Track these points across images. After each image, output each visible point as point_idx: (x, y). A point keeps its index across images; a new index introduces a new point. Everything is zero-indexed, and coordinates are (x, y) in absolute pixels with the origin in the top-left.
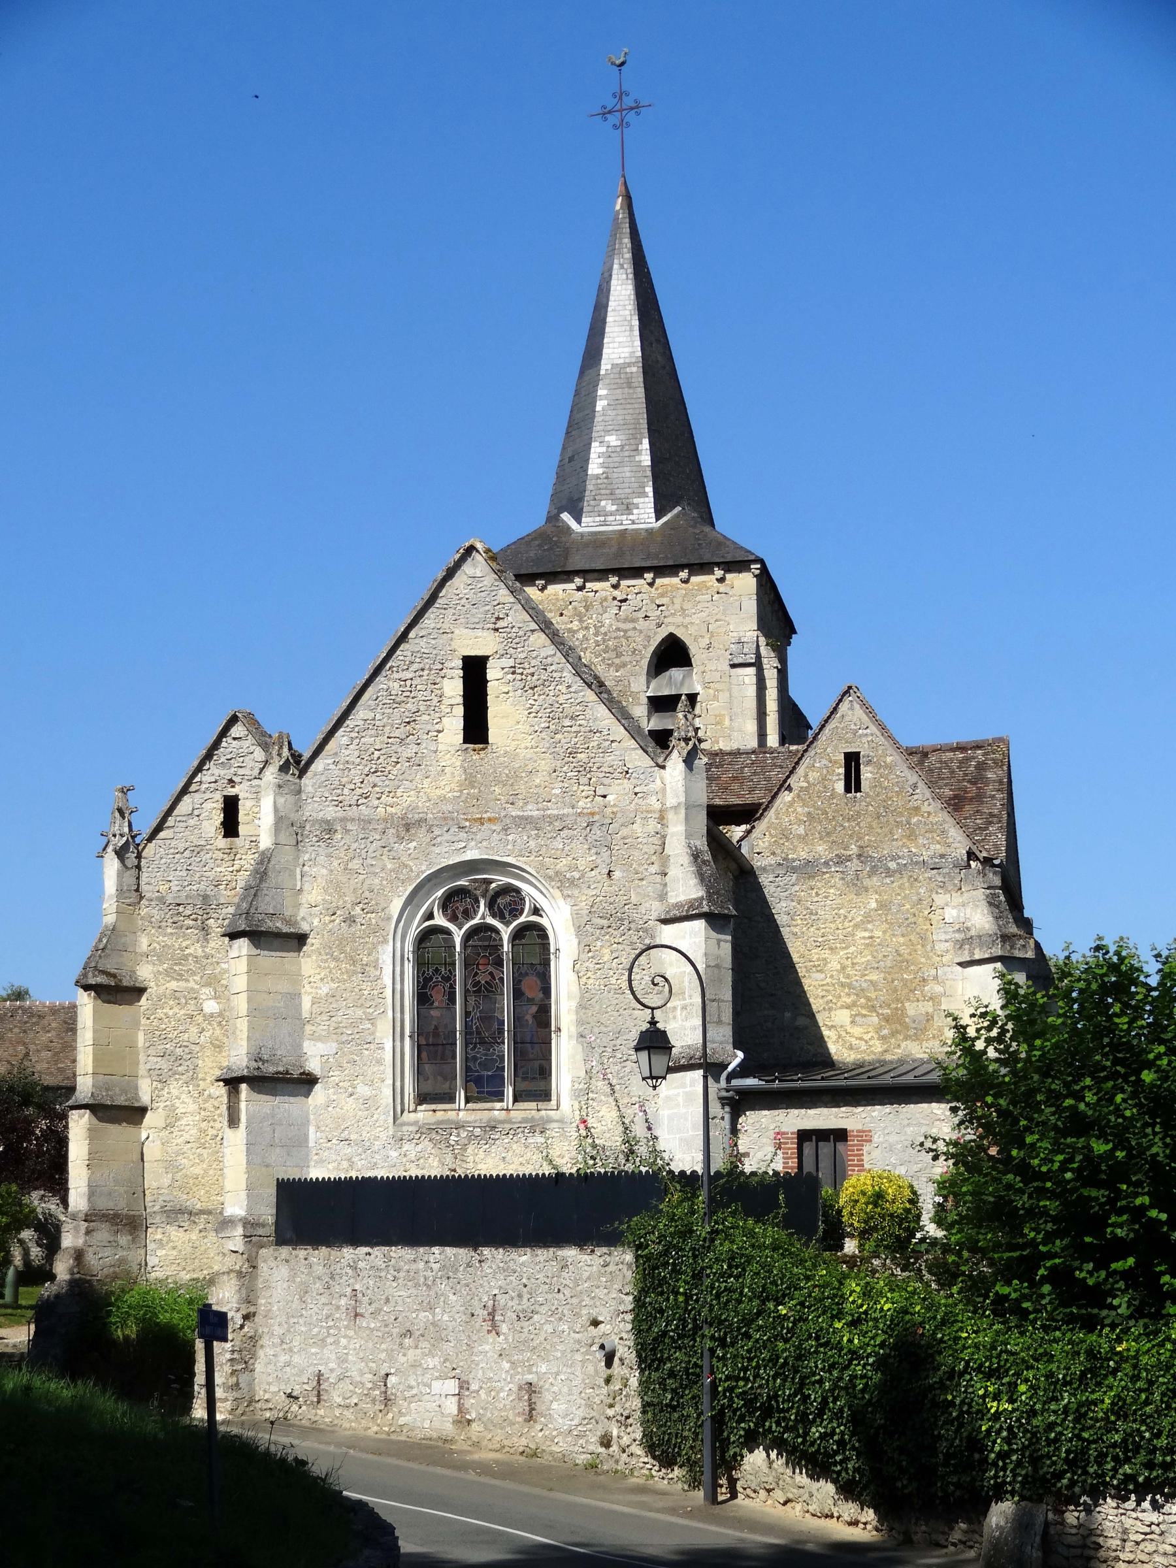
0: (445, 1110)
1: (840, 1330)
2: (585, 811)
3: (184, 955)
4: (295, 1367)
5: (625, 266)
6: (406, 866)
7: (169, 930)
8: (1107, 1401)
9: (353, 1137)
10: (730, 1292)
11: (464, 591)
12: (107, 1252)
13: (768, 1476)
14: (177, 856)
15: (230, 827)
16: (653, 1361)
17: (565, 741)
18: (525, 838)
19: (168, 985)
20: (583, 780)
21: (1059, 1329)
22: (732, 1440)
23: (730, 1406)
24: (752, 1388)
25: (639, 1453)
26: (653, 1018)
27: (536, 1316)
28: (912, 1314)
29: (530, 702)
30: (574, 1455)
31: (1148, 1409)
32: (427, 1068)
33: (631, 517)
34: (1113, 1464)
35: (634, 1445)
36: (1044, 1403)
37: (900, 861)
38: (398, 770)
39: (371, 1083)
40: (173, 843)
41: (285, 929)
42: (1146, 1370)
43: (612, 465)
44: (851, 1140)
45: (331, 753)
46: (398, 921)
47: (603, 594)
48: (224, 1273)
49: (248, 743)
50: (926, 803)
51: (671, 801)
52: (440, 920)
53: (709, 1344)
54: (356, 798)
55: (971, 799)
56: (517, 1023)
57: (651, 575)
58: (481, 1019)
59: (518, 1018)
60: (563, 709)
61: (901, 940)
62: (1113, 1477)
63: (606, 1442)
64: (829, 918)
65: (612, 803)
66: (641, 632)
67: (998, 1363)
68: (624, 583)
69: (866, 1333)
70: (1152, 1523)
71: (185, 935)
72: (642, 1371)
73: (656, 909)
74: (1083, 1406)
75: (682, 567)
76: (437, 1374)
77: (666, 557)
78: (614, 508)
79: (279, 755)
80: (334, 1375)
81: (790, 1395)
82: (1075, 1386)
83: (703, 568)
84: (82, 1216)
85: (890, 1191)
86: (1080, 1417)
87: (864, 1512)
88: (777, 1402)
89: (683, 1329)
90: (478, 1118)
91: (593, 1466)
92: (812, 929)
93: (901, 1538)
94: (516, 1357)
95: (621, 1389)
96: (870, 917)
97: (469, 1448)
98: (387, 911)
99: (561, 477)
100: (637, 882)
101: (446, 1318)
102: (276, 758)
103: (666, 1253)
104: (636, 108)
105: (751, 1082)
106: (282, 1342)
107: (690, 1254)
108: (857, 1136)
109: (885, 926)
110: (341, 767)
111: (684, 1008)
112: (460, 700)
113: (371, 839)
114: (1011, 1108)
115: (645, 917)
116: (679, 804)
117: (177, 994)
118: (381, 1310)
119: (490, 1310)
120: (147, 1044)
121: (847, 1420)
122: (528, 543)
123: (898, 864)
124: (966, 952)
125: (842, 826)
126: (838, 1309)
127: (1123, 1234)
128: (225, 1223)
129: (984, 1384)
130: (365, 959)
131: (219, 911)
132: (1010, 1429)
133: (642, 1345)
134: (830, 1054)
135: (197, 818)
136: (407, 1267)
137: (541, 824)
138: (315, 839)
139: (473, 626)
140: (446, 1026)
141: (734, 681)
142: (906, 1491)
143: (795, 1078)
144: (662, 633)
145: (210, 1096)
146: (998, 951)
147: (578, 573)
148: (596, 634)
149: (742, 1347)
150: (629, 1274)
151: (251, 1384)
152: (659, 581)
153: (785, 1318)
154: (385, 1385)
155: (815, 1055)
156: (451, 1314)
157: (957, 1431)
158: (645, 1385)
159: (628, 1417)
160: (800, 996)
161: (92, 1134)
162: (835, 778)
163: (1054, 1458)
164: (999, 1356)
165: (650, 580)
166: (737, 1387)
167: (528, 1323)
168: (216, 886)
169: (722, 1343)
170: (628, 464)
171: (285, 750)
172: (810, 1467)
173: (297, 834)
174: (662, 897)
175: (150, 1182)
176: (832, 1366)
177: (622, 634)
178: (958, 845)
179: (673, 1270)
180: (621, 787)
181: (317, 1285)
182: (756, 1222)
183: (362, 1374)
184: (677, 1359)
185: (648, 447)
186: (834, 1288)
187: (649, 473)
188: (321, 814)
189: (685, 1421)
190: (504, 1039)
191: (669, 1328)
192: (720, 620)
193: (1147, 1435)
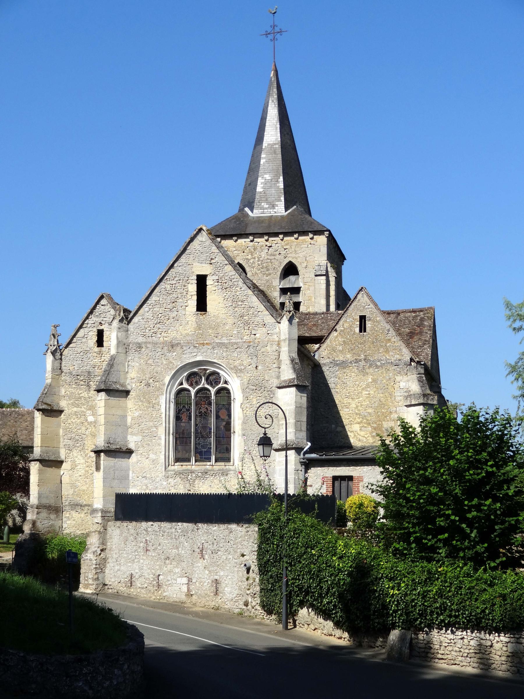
1: (335, 561)
2: (247, 341)
5: (274, 101)
6: (172, 363)
7: (74, 386)
8: (434, 591)
9: (148, 476)
10: (294, 544)
12: (46, 522)
13: (308, 618)
15: (100, 342)
16: (265, 571)
17: (239, 311)
18: (222, 352)
20: (246, 328)
21: (418, 562)
23: (293, 590)
24: (301, 583)
26: (265, 432)
28: (362, 555)
31: (450, 594)
33: (274, 210)
34: (436, 615)
36: (411, 591)
37: (382, 362)
38: (169, 322)
40: (76, 349)
41: (121, 388)
42: (450, 579)
43: (267, 188)
46: (168, 386)
47: (262, 243)
48: (93, 532)
49: (108, 307)
50: (393, 337)
51: (283, 337)
52: (185, 385)
53: (285, 565)
55: (417, 334)
56: (217, 429)
57: (282, 236)
61: (382, 395)
62: (436, 621)
63: (246, 604)
64: (352, 386)
66: (277, 260)
67: (394, 575)
68: (271, 239)
69: (345, 562)
70: (451, 639)
72: (260, 575)
73: (276, 382)
74: (425, 592)
75: (295, 233)
78: (267, 206)
79: (119, 315)
80: (137, 575)
81: (315, 586)
82: (422, 584)
83: (304, 233)
84: (35, 506)
85: (366, 503)
86: (424, 597)
87: (344, 634)
88: (311, 589)
89: (276, 558)
90: (200, 469)
91: (241, 614)
92: (344, 390)
93: (358, 644)
96: (368, 385)
97: (192, 606)
99: (245, 192)
101: (183, 552)
102: (118, 317)
104: (280, 32)
105: (313, 456)
108: (357, 479)
109: (375, 389)
110: (145, 320)
112: (195, 293)
113: (157, 351)
114: (401, 473)
115: (271, 386)
117: (76, 413)
118: (157, 548)
120: (64, 435)
121: (337, 597)
122: (230, 221)
123: (381, 363)
124: (409, 401)
125: (358, 346)
126: (335, 552)
127: (443, 525)
128: (94, 511)
129: (388, 583)
131: (95, 378)
132: (398, 601)
134: (351, 443)
136: (168, 531)
137: (228, 346)
138: (134, 351)
139: (201, 262)
140: (187, 430)
141: (316, 282)
142: (359, 625)
143: (332, 454)
144: (286, 261)
145: (90, 456)
146: (421, 401)
147: (251, 234)
148: (258, 261)
150: (256, 535)
151: (104, 578)
152: (285, 238)
153: (315, 555)
154: (158, 579)
155: (344, 443)
157: (378, 602)
158: (261, 581)
159: (255, 594)
160: (338, 418)
161: (40, 472)
162: (355, 326)
163: (414, 613)
164: (394, 572)
165: (281, 238)
166: (296, 582)
169: (291, 565)
170: (274, 187)
172: (323, 615)
174: (278, 377)
175: (64, 492)
176: (332, 575)
177: (269, 261)
178: (407, 355)
179: (273, 535)
182: (306, 516)
184: (273, 571)
185: (282, 180)
186: (334, 544)
187: (283, 191)
188: (136, 340)
189: (277, 596)
190: (211, 436)
192: (311, 256)
193: (449, 604)
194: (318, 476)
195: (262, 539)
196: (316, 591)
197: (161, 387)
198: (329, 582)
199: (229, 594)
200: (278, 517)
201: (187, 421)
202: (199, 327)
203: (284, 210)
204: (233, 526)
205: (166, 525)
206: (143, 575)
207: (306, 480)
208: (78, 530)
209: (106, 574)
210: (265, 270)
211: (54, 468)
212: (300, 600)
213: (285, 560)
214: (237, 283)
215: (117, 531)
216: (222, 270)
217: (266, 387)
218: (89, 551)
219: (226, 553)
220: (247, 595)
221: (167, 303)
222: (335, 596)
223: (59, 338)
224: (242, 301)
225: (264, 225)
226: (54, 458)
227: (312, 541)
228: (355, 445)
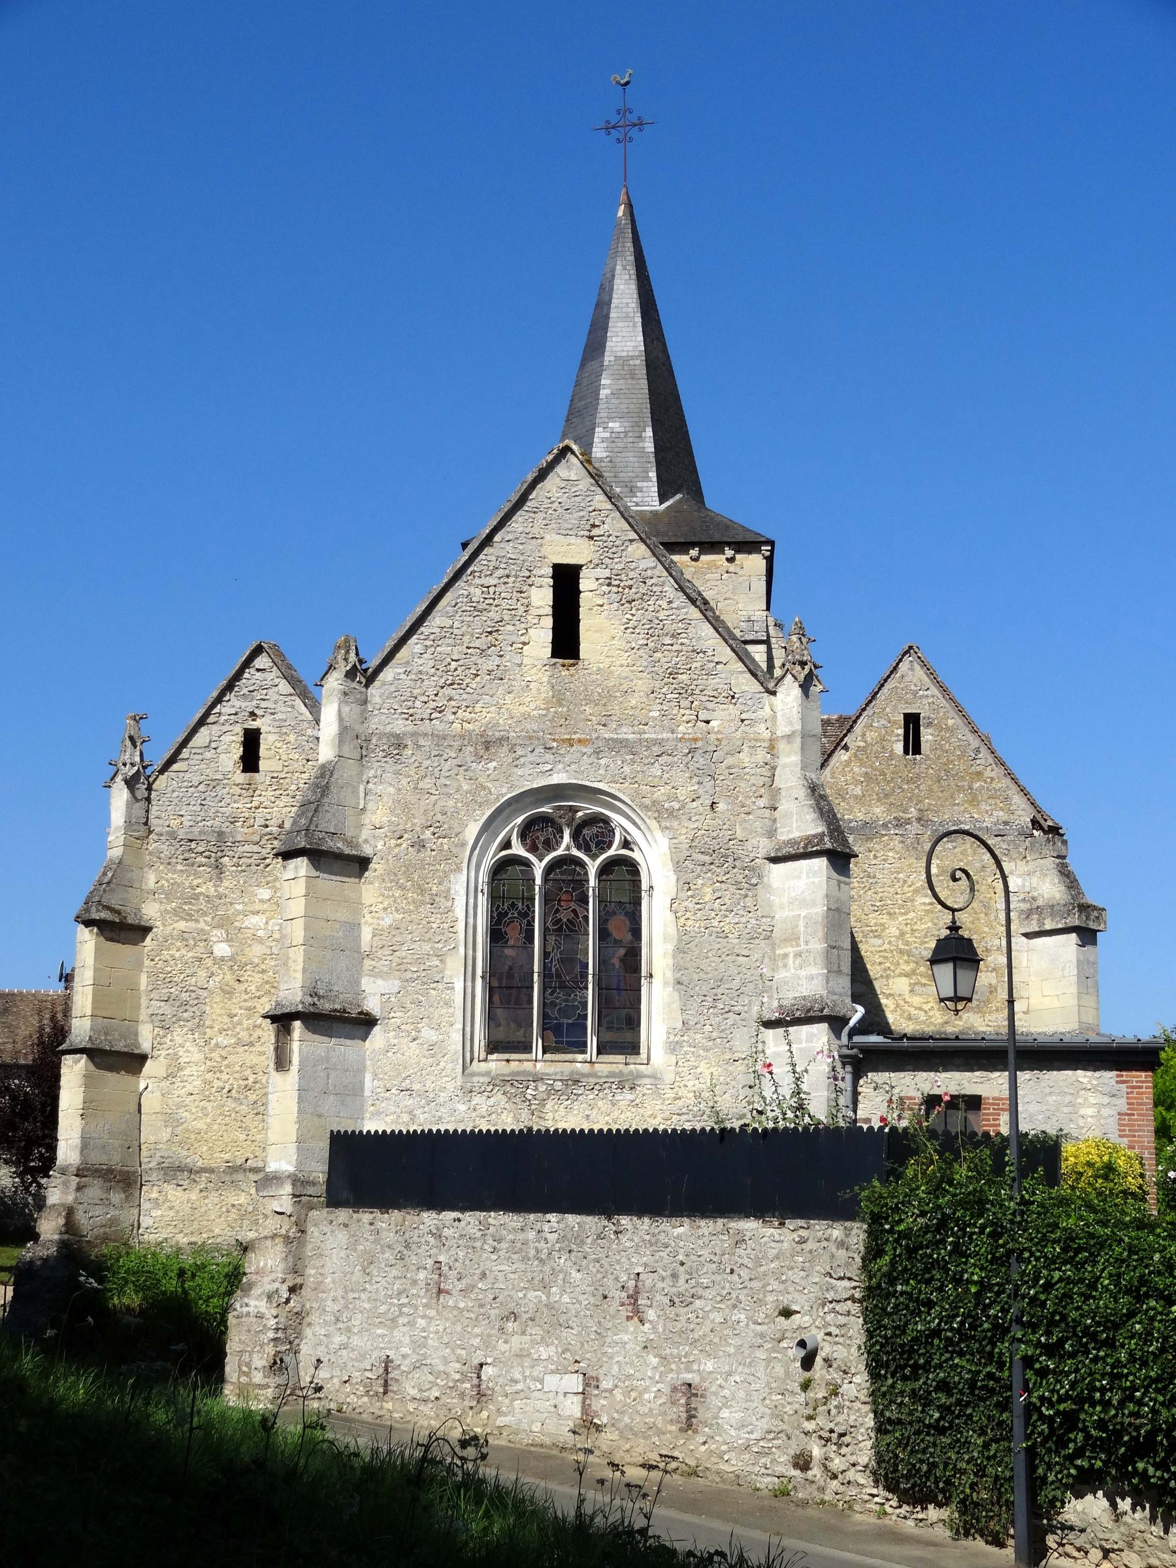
0: (519, 1061)
2: (687, 736)
3: (194, 894)
4: (353, 1350)
5: (628, 267)
6: (484, 788)
7: (179, 867)
9: (416, 1087)
11: (556, 494)
12: (98, 1211)
14: (190, 790)
15: (250, 760)
18: (619, 763)
19: (176, 925)
25: (862, 1481)
26: (954, 922)
27: (697, 1301)
29: (627, 616)
30: (753, 1477)
32: (499, 1012)
33: (634, 499)
40: (187, 775)
41: (347, 851)
43: (616, 450)
44: (985, 1109)
45: (402, 662)
48: (266, 1238)
49: (273, 675)
50: (989, 768)
51: (783, 729)
52: (518, 849)
54: (429, 711)
59: (604, 961)
60: (664, 625)
63: (802, 1462)
64: (889, 882)
65: (716, 730)
73: (765, 846)
75: (693, 545)
76: (553, 1367)
79: (346, 660)
83: (712, 547)
84: (73, 1170)
92: (870, 893)
100: (743, 815)
102: (343, 663)
108: (993, 1104)
110: (413, 677)
111: (798, 955)
112: (549, 611)
113: (445, 757)
115: (752, 855)
116: (793, 733)
117: (185, 935)
118: (474, 1287)
119: (631, 1292)
120: (150, 988)
124: (1034, 922)
125: (901, 788)
128: (269, 1180)
130: (435, 888)
136: (511, 1237)
137: (637, 749)
139: (566, 532)
145: (217, 1045)
146: (1075, 920)
154: (479, 1377)
156: (572, 1295)
161: (89, 1082)
162: (894, 739)
167: (686, 1309)
171: (352, 655)
173: (361, 748)
174: (771, 833)
175: (147, 1136)
180: (727, 712)
181: (387, 1255)
187: (653, 459)
188: (388, 729)
192: (730, 599)
197: (454, 850)
199: (738, 1429)
203: (657, 499)
204: (750, 1226)
205: (502, 1221)
206: (429, 1362)
208: (182, 1235)
211: (123, 1073)
214: (660, 589)
215: (340, 1236)
218: (255, 1292)
219: (723, 1306)
224: (673, 636)
226: (125, 1047)
228: (898, 1028)
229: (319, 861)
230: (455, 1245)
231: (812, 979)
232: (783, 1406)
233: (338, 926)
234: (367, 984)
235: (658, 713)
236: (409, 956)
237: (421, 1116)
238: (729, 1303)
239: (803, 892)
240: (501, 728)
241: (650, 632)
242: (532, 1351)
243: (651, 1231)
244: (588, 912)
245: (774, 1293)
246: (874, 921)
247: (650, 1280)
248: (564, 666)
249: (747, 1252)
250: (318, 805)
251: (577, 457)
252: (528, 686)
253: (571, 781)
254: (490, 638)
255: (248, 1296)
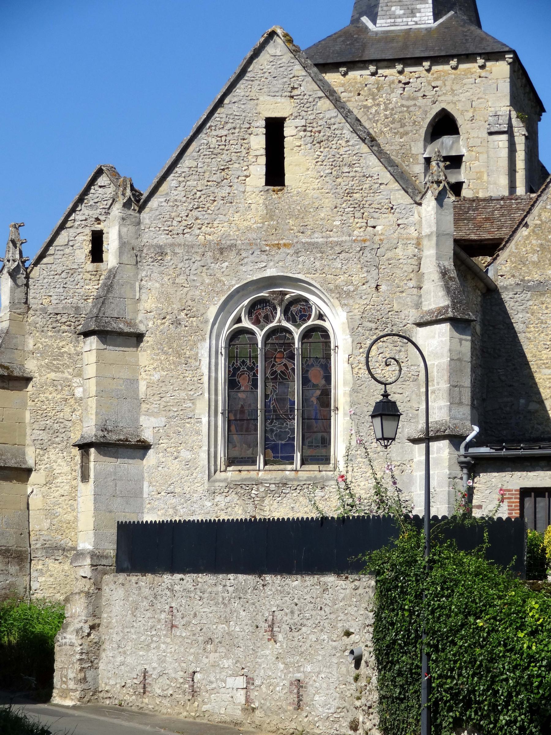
0: (248, 471)
2: (359, 238)
3: (60, 353)
4: (128, 666)
6: (220, 281)
7: (50, 334)
9: (177, 490)
10: (442, 609)
11: (267, 67)
16: (387, 663)
18: (312, 259)
19: (48, 375)
20: (358, 214)
22: (444, 725)
23: (442, 699)
24: (456, 684)
26: (386, 391)
27: (303, 628)
29: (317, 153)
32: (235, 438)
33: (414, 19)
35: (374, 729)
39: (192, 449)
40: (54, 267)
41: (126, 329)
45: (163, 193)
48: (76, 593)
51: (426, 231)
52: (246, 323)
53: (426, 650)
54: (182, 228)
58: (277, 400)
59: (306, 400)
65: (380, 233)
66: (420, 107)
68: (408, 70)
69: (542, 641)
71: (61, 337)
72: (380, 671)
73: (413, 315)
75: (452, 57)
76: (231, 672)
77: (440, 50)
78: (402, 12)
79: (123, 194)
80: (155, 672)
81: (484, 690)
83: (468, 57)
88: (475, 695)
90: (273, 477)
92: (542, 335)
94: (288, 660)
95: (366, 686)
97: (253, 730)
98: (205, 316)
100: (398, 294)
101: (237, 629)
102: (121, 197)
103: (396, 578)
106: (119, 647)
107: (414, 579)
110: (171, 204)
112: (263, 152)
113: (193, 260)
115: (404, 322)
116: (432, 233)
117: (55, 382)
118: (190, 622)
119: (270, 623)
120: (32, 421)
122: (335, 40)
126: (522, 622)
128: (79, 555)
130: (188, 353)
133: (379, 650)
135: (71, 248)
136: (209, 590)
138: (150, 260)
139: (273, 94)
140: (250, 405)
141: (491, 146)
147: (371, 62)
149: (450, 652)
151: (95, 679)
152: (434, 68)
153: (482, 629)
154: (193, 681)
155: (543, 433)
156: (241, 626)
158: (382, 681)
159: (370, 707)
160: (531, 387)
165: (427, 68)
166: (445, 683)
167: (297, 633)
168: (85, 300)
169: (437, 650)
173: (136, 256)
174: (418, 306)
176: (516, 667)
177: (405, 109)
179: (402, 592)
180: (387, 220)
181: (145, 603)
183: (176, 672)
184: (403, 662)
186: (519, 606)
188: (155, 241)
189: (410, 710)
190: (294, 416)
191: (398, 637)
192: (482, 98)
194: (494, 488)
195: (381, 601)
196: (486, 700)
197: (200, 326)
198: (511, 681)
200: (412, 557)
201: (249, 389)
202: (270, 214)
203: (432, 17)
204: (330, 579)
206: (167, 672)
207: (470, 491)
208: (59, 594)
209: (100, 671)
210: (397, 125)
211: (15, 481)
212: (455, 719)
213: (425, 639)
215: (120, 591)
216: (311, 108)
217: (395, 324)
218: (70, 629)
219: (316, 631)
220: (356, 708)
221: (211, 172)
222: (522, 708)
223: (24, 248)
225: (394, 45)
226: (16, 463)
227: (477, 601)
229: (106, 338)
230: (181, 596)
231: (441, 408)
232: (346, 692)
233: (121, 382)
234: (144, 421)
235: (339, 222)
236: (172, 401)
237: (181, 510)
238: (319, 628)
239: (436, 348)
240: (231, 238)
241: (333, 163)
242: (220, 663)
243: (281, 584)
244: (294, 365)
245: (342, 622)
246: (546, 356)
247: (280, 615)
248: (274, 191)
249: (329, 596)
250: (104, 299)
251: (280, 37)
252: (249, 207)
253: (279, 274)
254: (223, 173)
255: (65, 632)
